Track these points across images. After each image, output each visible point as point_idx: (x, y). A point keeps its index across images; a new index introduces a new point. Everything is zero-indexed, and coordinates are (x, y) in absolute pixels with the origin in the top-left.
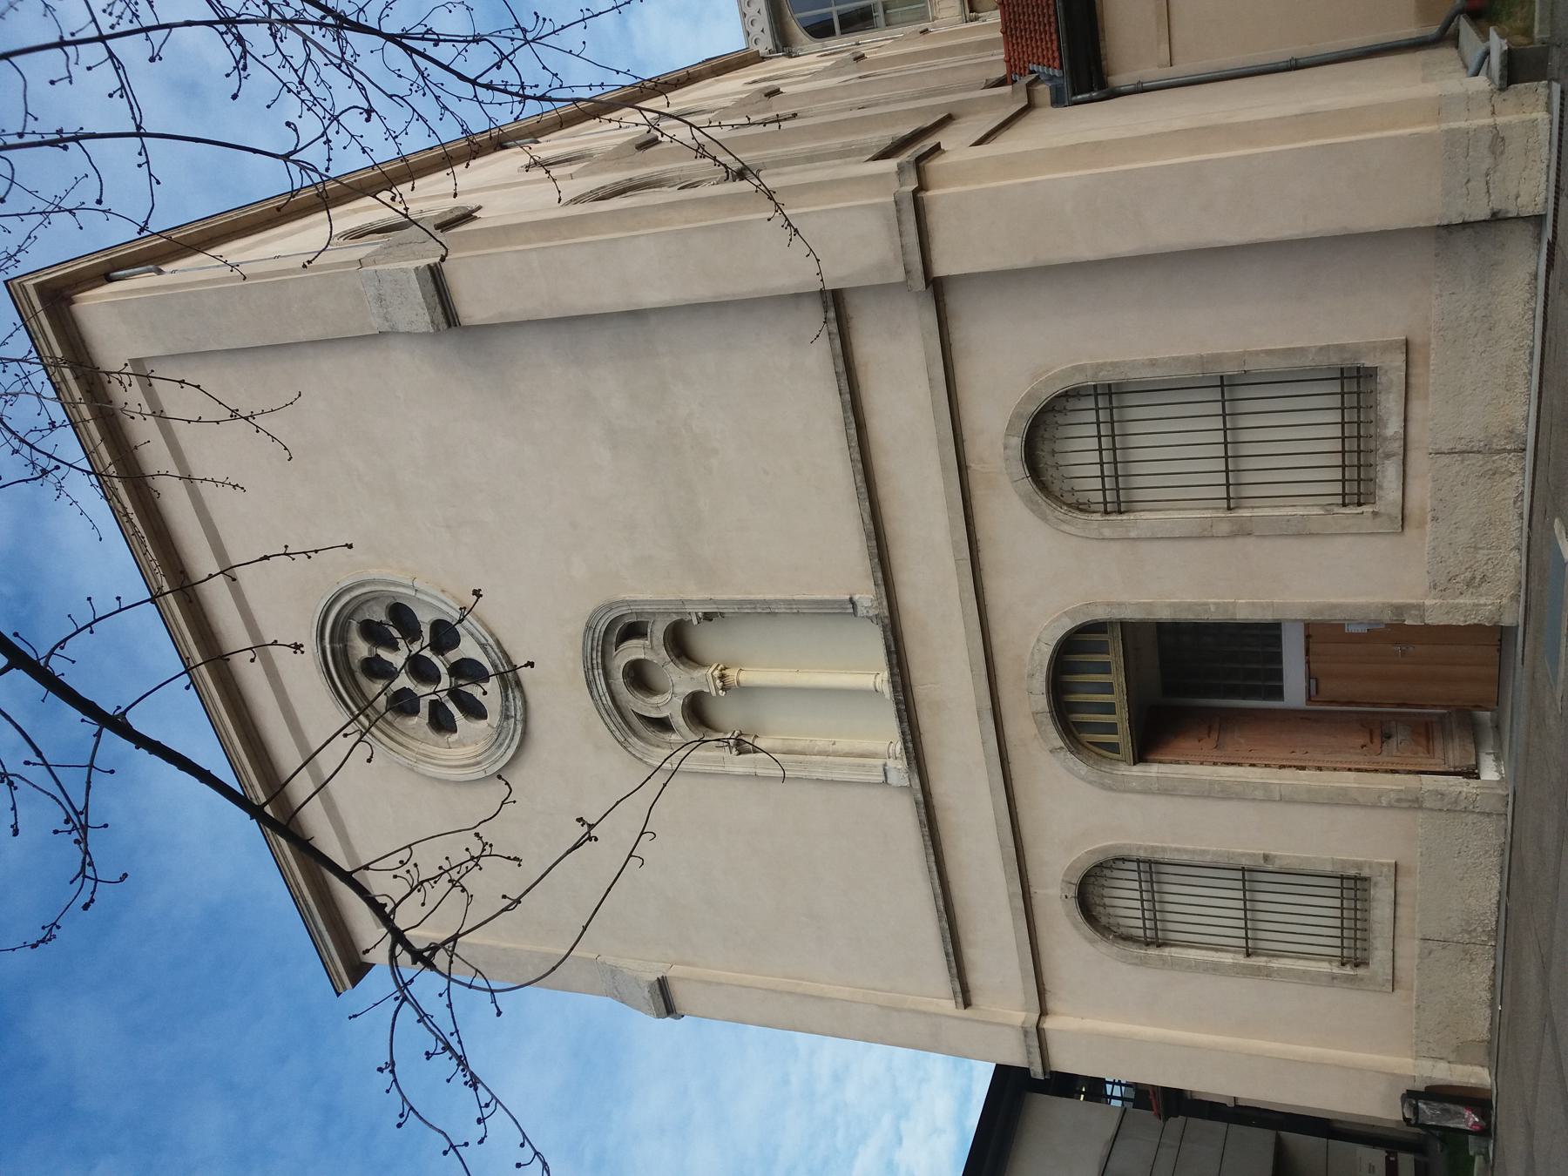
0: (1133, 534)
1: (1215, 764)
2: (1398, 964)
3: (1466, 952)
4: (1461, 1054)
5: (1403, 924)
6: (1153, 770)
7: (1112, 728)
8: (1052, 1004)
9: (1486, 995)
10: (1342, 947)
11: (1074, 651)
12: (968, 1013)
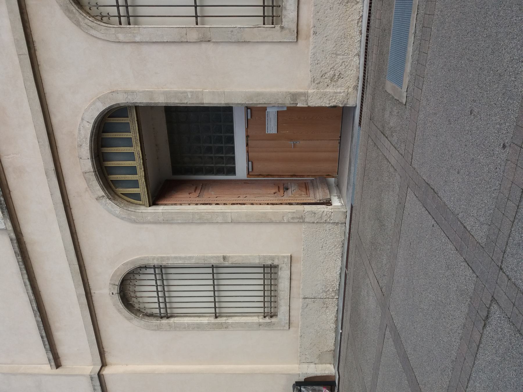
0: (138, 39)
1: (197, 204)
2: (291, 314)
3: (324, 303)
4: (321, 359)
5: (294, 290)
6: (160, 209)
7: (135, 184)
8: (109, 359)
9: (333, 326)
10: (264, 307)
11: (107, 126)
12: (59, 370)
